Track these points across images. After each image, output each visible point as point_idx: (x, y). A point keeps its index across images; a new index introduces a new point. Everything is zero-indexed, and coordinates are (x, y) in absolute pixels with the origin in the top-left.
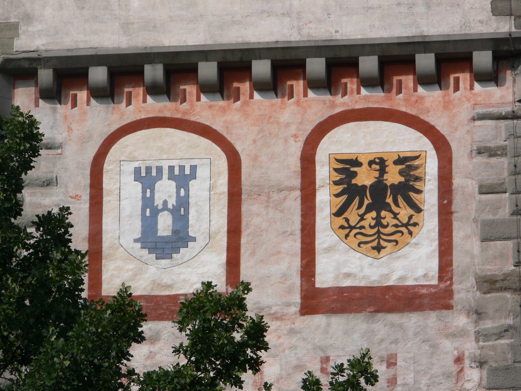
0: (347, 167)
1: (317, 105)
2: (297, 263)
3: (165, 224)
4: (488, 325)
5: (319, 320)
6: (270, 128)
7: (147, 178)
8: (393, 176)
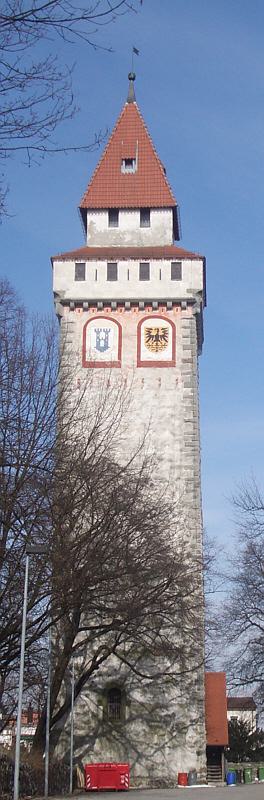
0: (149, 331)
1: (86, 316)
2: (202, 277)
3: (102, 344)
4: (184, 371)
5: (141, 369)
6: (130, 319)
7: (98, 332)
8: (161, 333)
